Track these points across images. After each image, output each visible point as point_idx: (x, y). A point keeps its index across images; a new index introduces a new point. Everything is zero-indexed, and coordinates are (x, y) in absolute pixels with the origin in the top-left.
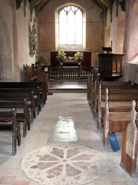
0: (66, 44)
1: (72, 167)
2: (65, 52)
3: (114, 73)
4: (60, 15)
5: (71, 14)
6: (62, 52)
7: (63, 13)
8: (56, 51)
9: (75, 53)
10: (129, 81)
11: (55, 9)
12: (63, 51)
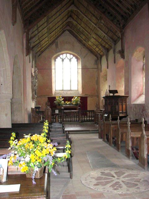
0: (62, 89)
1: (128, 182)
2: (63, 97)
3: (121, 113)
4: (56, 62)
5: (66, 61)
6: (60, 97)
7: (59, 60)
8: (53, 96)
9: (72, 97)
10: (136, 119)
11: (52, 57)
12: (61, 96)
